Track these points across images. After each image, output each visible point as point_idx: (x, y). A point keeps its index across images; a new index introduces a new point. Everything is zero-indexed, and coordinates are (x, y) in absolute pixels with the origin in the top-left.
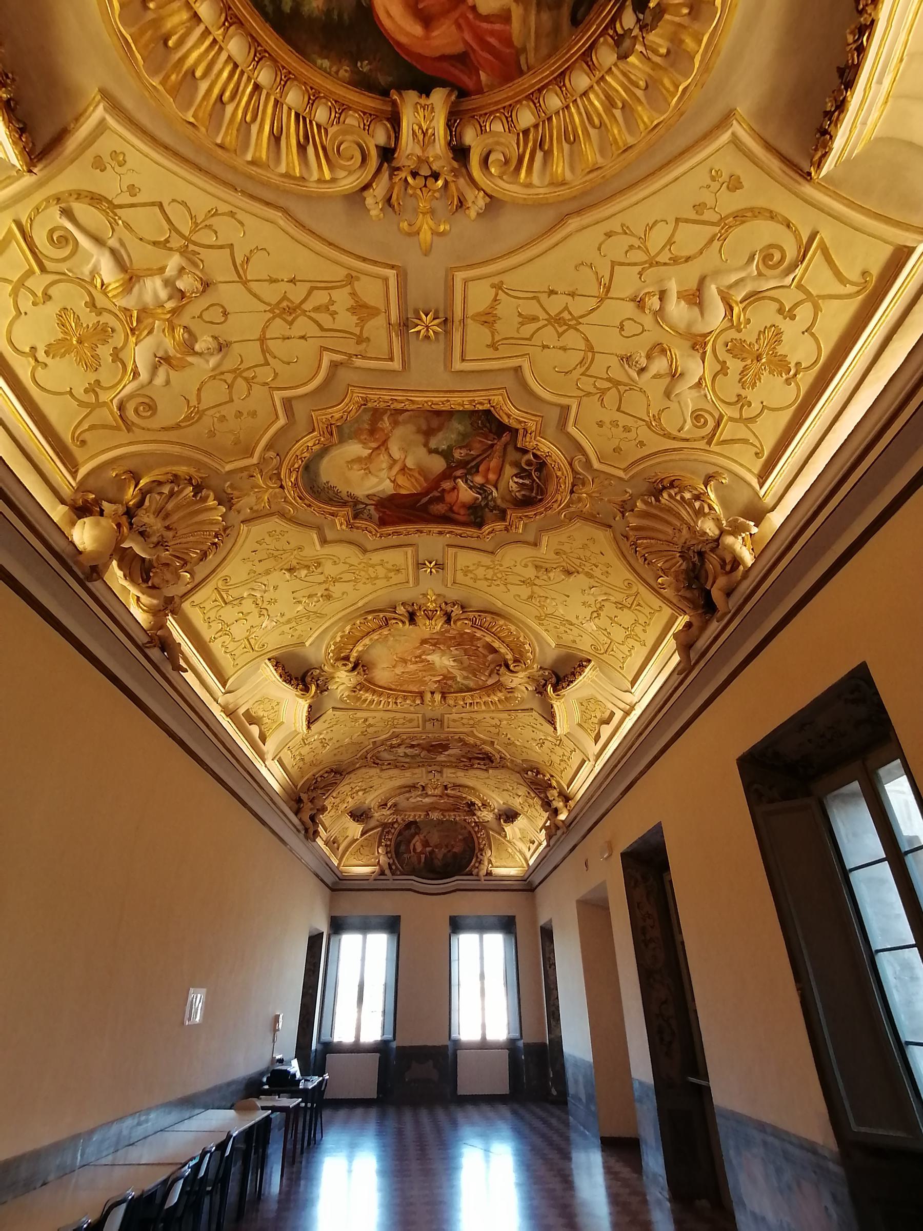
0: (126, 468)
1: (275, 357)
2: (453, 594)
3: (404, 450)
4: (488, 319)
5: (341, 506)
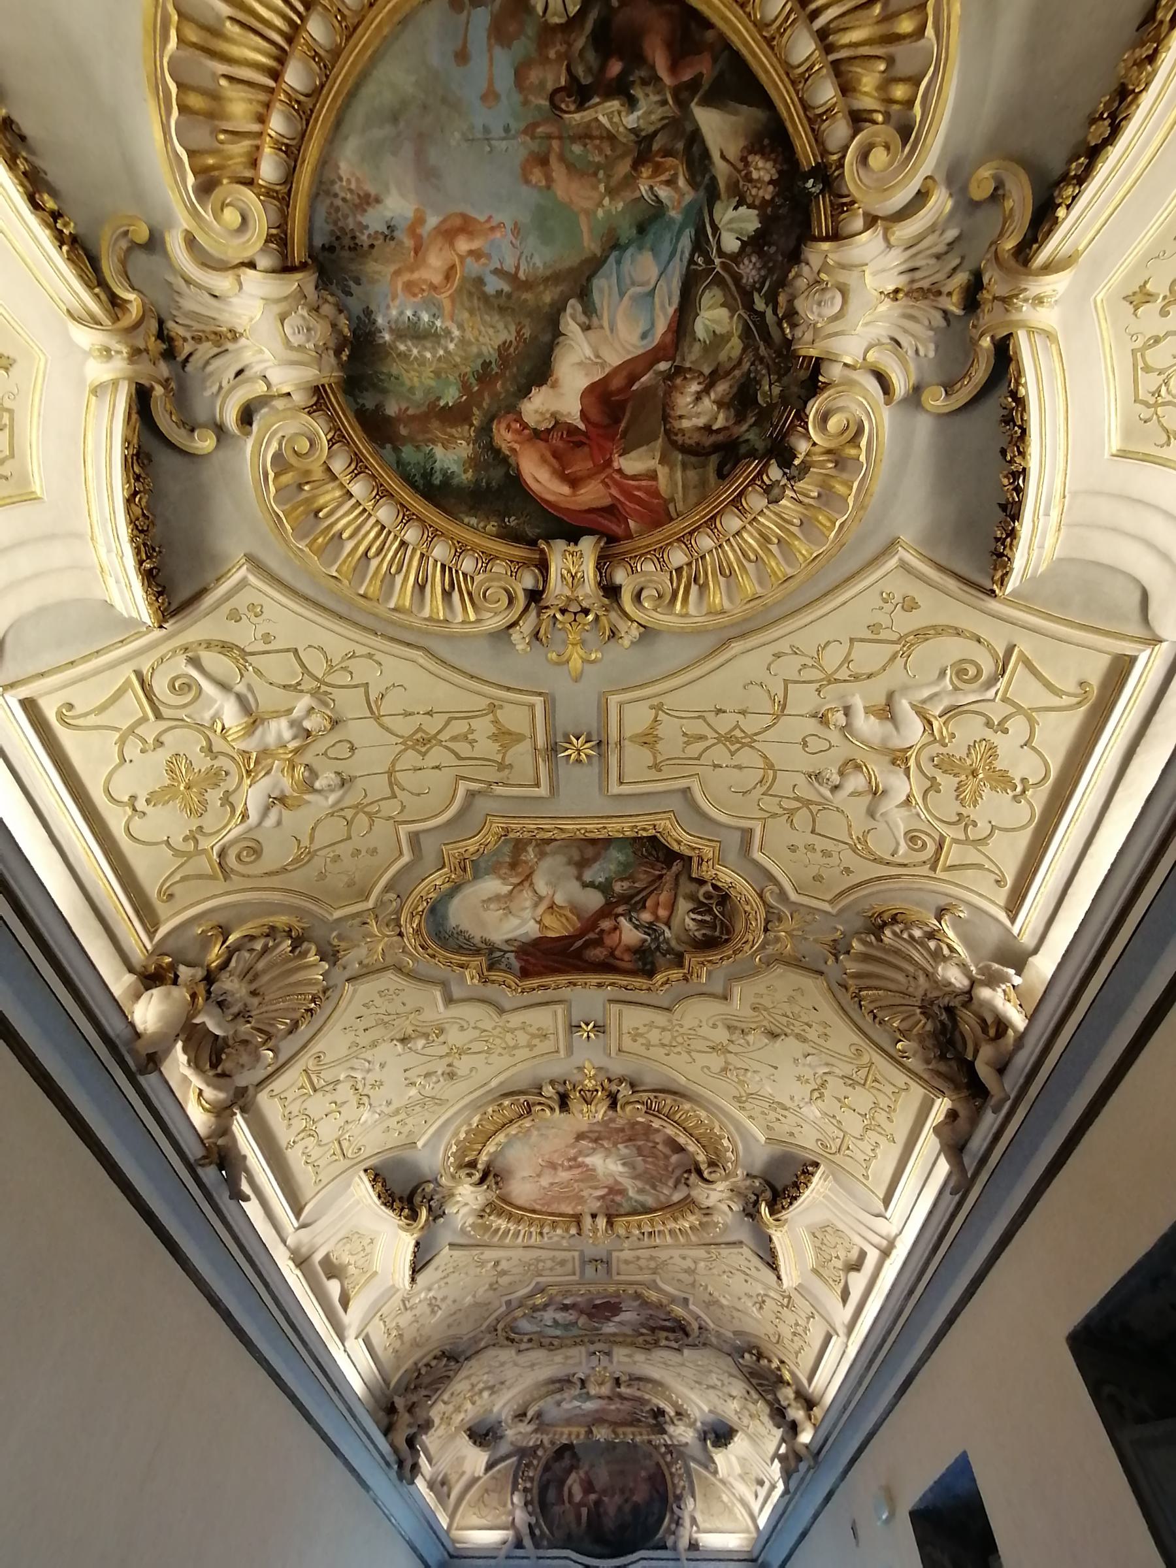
0: (214, 923)
2: (618, 1067)
3: (554, 885)
4: (648, 739)
5: (474, 955)
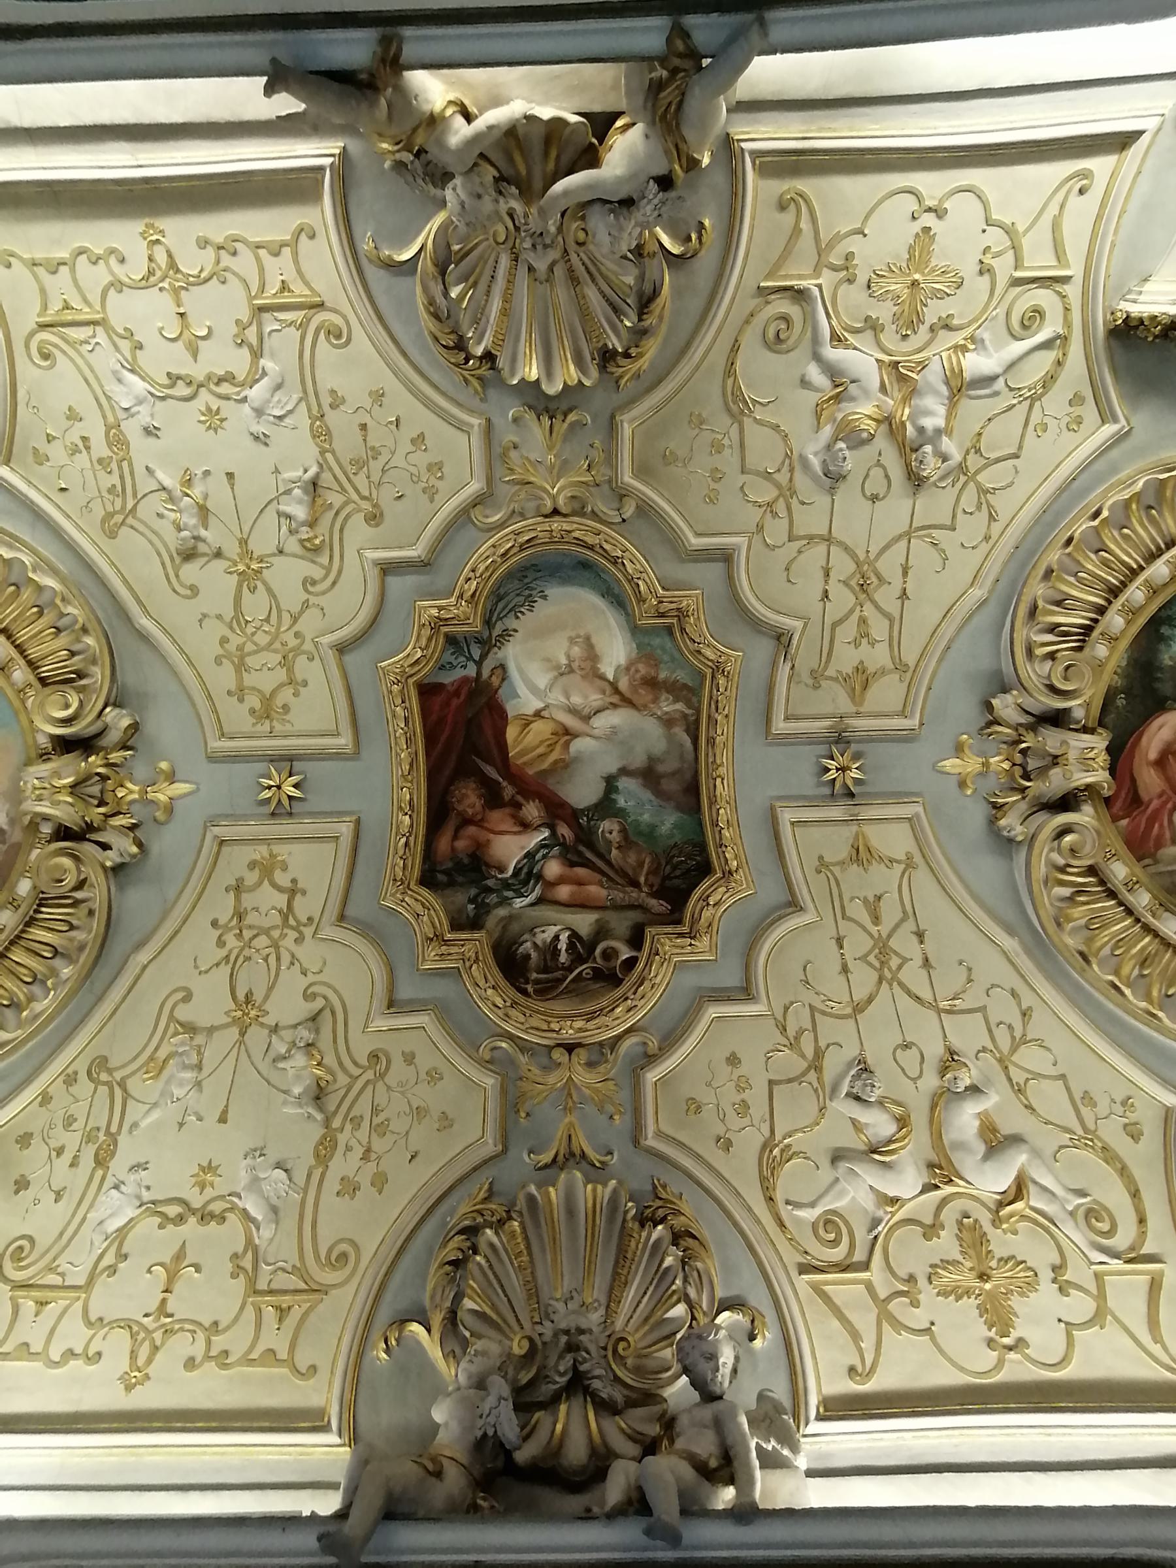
1: (800, 552)
4: (861, 854)
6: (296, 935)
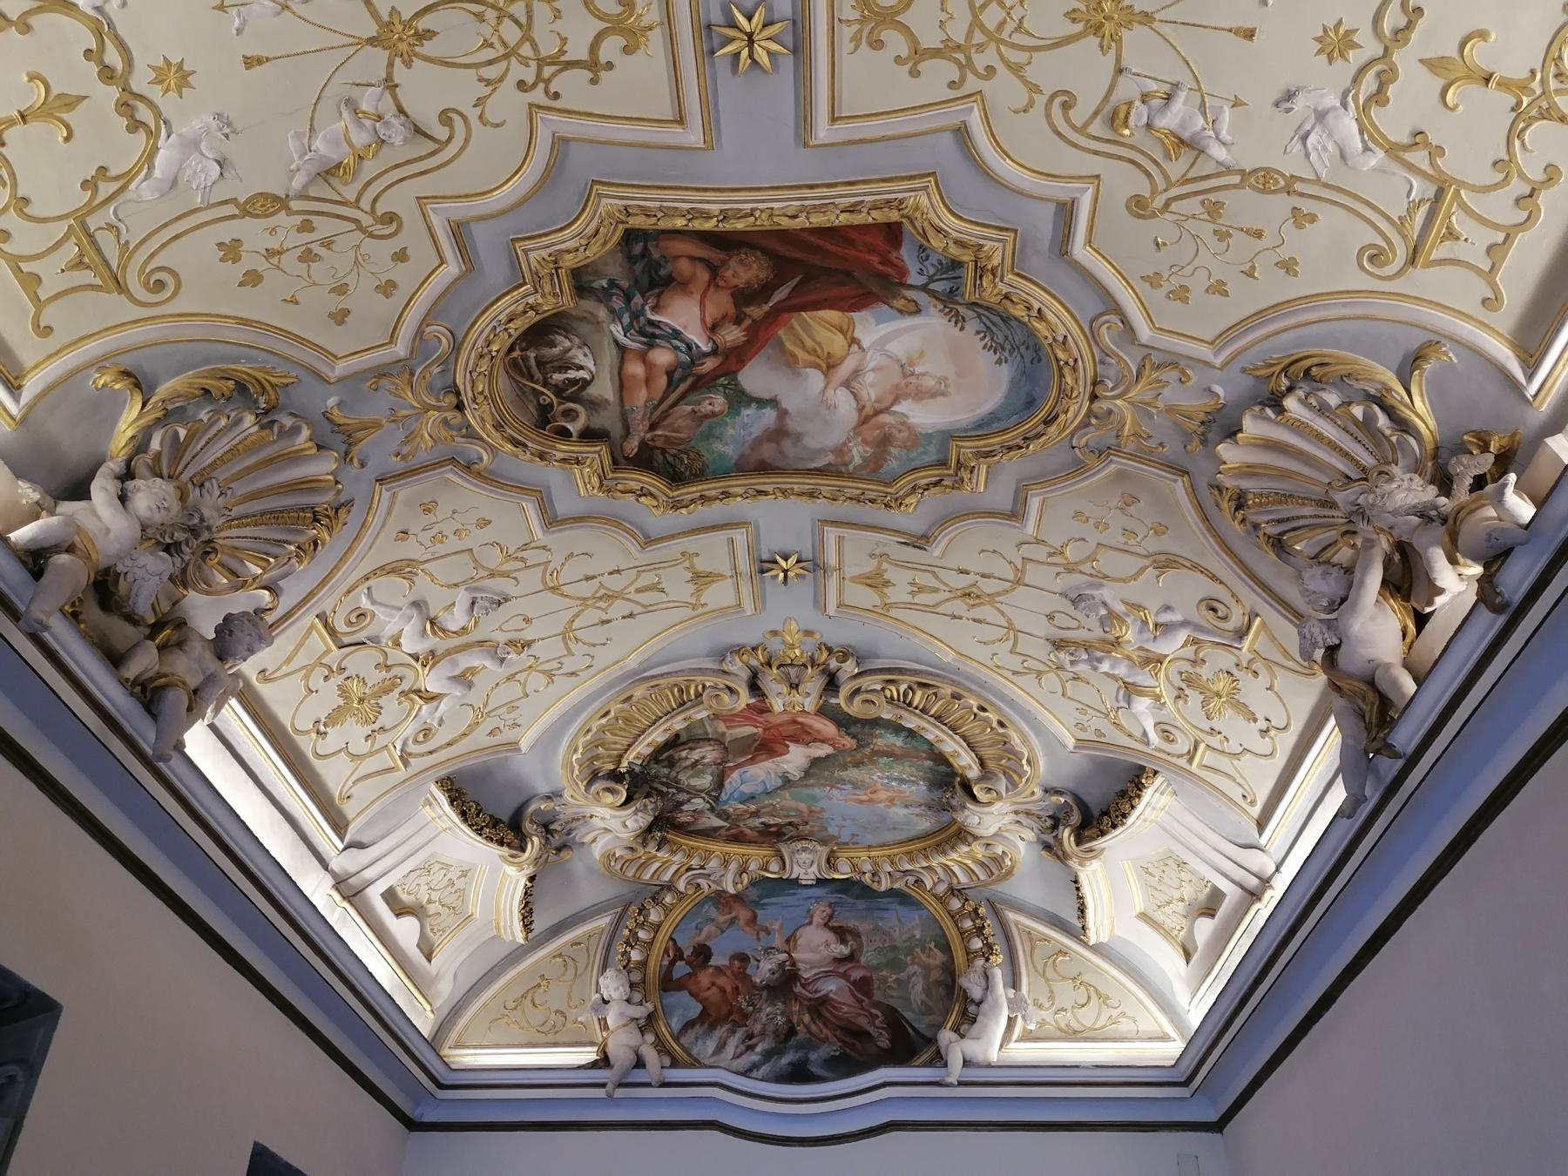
3: (823, 401)
6: (530, 80)
